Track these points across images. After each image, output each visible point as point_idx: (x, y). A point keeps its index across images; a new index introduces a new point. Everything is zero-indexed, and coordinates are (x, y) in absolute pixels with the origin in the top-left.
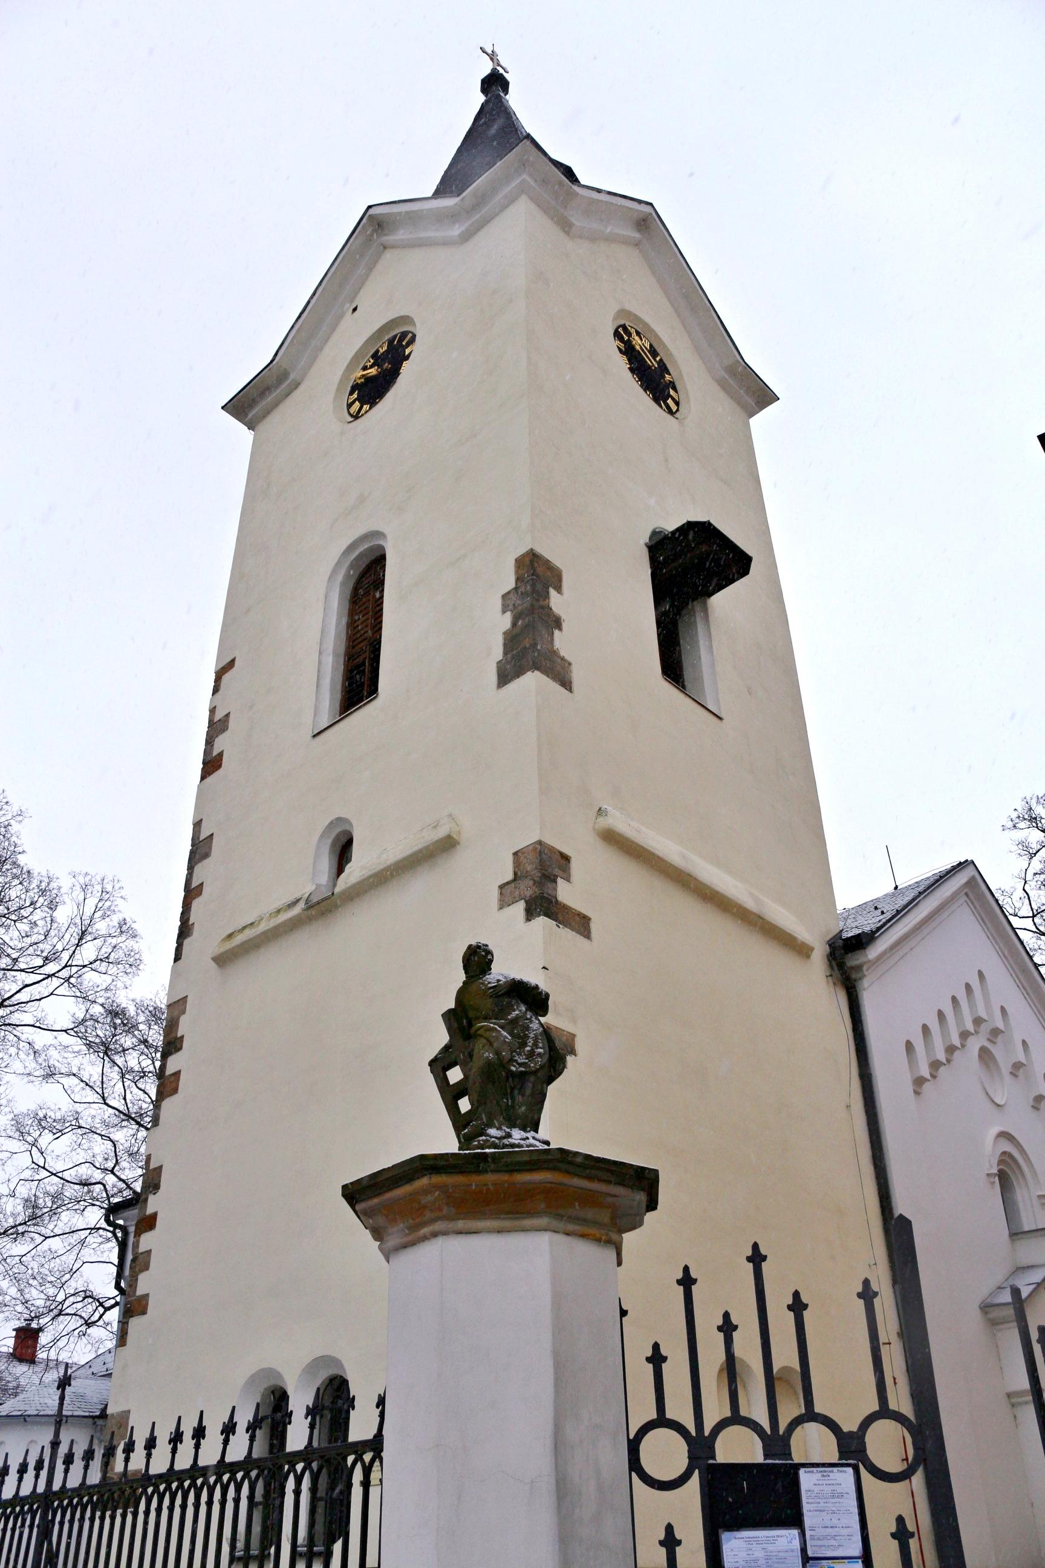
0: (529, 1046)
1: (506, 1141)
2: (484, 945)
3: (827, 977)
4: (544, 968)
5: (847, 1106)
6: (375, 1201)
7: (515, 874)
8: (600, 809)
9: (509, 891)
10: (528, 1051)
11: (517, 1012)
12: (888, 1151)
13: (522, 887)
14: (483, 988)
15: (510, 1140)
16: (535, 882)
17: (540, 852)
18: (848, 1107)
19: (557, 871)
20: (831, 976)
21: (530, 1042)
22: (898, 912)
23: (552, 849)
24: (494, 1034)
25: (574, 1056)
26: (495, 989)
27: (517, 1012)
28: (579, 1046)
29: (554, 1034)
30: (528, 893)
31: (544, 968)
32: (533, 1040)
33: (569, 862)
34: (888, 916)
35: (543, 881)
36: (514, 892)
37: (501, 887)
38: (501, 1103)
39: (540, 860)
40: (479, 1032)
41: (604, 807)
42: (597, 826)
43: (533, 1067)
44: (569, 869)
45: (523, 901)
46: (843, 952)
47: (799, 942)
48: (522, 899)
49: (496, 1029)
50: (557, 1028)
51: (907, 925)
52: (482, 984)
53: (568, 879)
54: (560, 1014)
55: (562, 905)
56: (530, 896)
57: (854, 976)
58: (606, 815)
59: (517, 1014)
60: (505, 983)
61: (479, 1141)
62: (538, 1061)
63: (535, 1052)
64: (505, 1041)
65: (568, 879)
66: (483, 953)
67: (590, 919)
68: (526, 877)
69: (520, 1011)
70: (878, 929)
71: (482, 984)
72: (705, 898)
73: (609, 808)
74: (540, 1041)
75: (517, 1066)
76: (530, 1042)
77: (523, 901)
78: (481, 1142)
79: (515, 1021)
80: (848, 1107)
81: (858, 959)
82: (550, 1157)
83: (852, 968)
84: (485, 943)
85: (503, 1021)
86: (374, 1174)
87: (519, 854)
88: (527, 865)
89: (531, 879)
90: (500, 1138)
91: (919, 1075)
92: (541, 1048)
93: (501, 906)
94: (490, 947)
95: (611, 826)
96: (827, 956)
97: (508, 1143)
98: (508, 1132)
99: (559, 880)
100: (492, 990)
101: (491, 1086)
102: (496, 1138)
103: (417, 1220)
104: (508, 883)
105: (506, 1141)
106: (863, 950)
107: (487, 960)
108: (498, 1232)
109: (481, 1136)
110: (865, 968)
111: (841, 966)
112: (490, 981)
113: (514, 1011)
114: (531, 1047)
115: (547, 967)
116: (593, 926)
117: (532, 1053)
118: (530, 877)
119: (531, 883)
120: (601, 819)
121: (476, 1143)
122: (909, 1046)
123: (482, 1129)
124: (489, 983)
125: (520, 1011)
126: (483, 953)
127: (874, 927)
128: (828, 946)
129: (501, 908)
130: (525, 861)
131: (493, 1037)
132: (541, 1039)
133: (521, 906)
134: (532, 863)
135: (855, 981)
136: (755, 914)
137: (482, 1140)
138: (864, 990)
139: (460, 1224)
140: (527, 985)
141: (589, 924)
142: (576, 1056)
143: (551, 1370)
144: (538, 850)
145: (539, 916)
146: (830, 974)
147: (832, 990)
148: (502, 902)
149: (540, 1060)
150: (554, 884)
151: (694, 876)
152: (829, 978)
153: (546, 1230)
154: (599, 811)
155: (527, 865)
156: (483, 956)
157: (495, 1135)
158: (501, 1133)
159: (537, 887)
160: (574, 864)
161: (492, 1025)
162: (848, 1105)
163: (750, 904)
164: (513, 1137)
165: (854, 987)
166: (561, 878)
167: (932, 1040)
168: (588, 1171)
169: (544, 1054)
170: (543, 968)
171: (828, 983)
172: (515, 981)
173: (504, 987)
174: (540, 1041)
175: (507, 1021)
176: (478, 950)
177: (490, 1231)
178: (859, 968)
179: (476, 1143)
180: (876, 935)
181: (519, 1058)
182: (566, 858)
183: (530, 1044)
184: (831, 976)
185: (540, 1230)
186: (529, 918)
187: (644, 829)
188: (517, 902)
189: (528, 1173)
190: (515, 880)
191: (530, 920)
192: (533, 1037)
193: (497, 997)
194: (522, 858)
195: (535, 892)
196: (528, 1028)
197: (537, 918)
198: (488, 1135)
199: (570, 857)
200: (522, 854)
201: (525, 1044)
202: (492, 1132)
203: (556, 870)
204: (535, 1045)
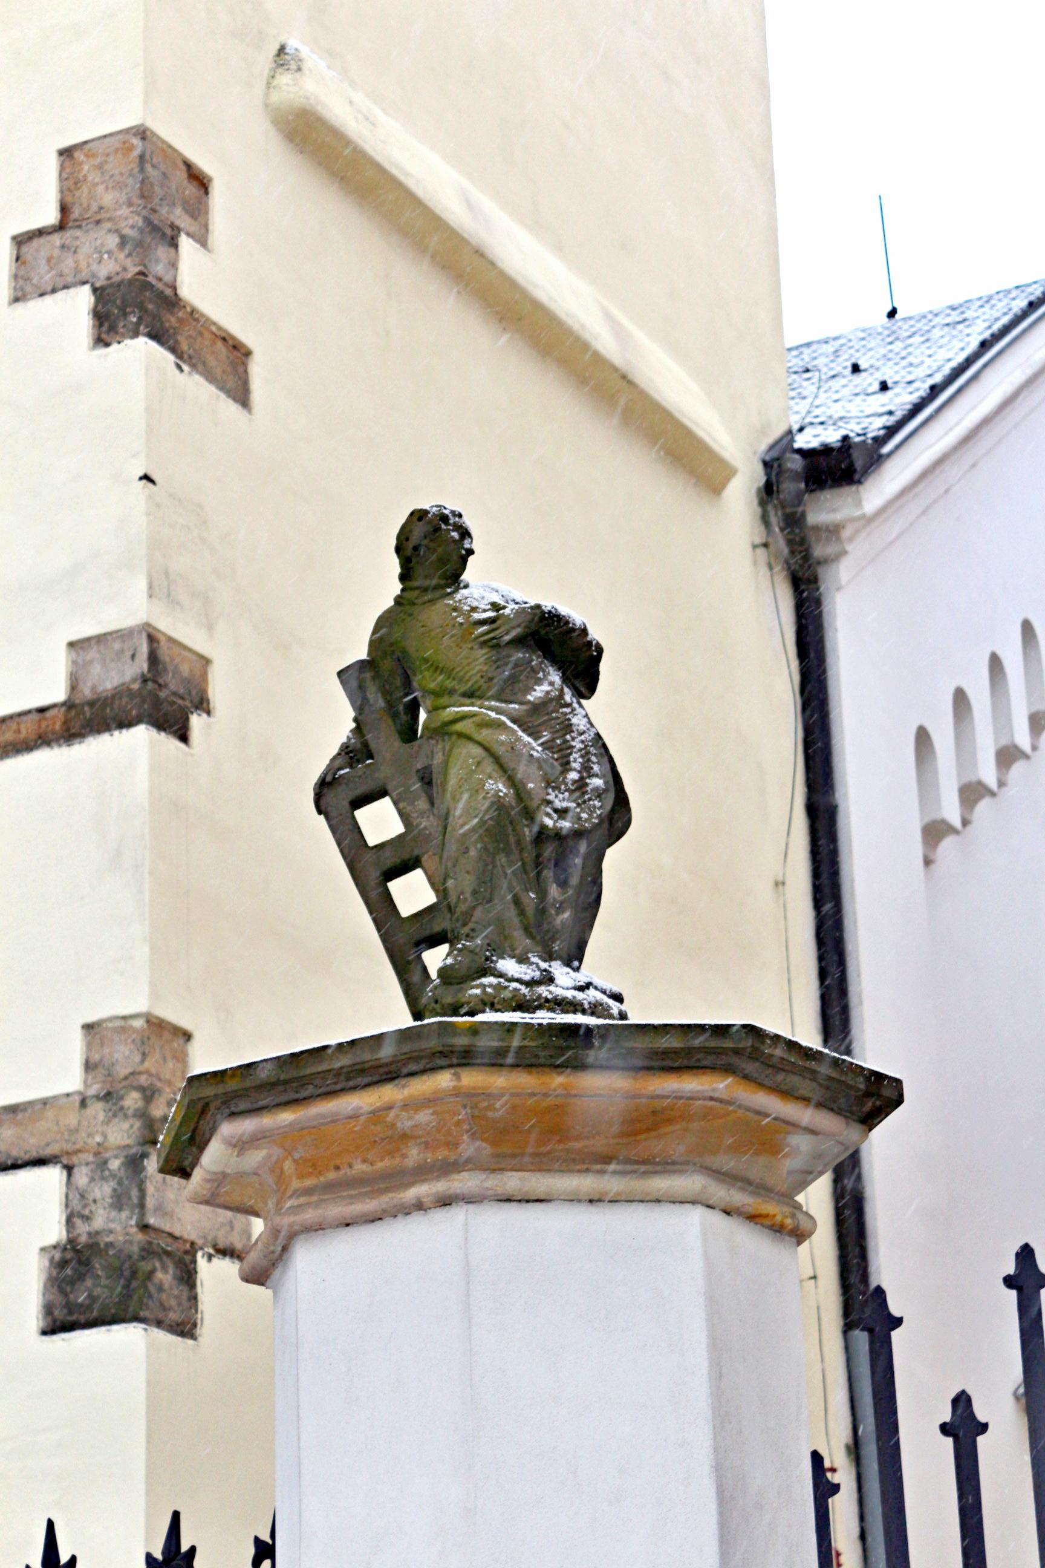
0: (575, 770)
1: (543, 991)
2: (453, 512)
3: (755, 547)
4: (146, 477)
5: (777, 884)
6: (286, 1117)
7: (64, 209)
8: (282, 50)
9: (44, 254)
10: (575, 782)
11: (545, 687)
12: (861, 1003)
13: (85, 250)
14: (460, 620)
15: (552, 988)
16: (124, 241)
17: (142, 157)
18: (779, 884)
19: (183, 220)
20: (765, 545)
21: (576, 764)
22: (935, 391)
23: (168, 151)
24: (503, 738)
25: (205, 715)
26: (493, 626)
27: (545, 687)
28: (218, 690)
29: (165, 652)
30: (106, 270)
31: (146, 477)
32: (582, 756)
33: (207, 193)
34: (901, 399)
35: (148, 239)
36: (60, 260)
37: (21, 241)
38: (525, 901)
39: (142, 182)
40: (459, 727)
41: (292, 44)
42: (275, 98)
43: (586, 820)
44: (207, 213)
45: (87, 288)
46: (803, 486)
47: (844, 483)
48: (84, 283)
49: (504, 723)
50: (171, 640)
51: (951, 429)
52: (455, 609)
53: (203, 241)
54: (178, 603)
55: (189, 309)
56: (109, 278)
57: (818, 551)
58: (299, 69)
59: (548, 693)
60: (519, 613)
61: (483, 986)
62: (594, 807)
63: (587, 785)
64: (532, 755)
65: (203, 241)
66: (455, 535)
67: (248, 353)
68: (98, 222)
69: (552, 684)
70: (891, 431)
71: (455, 609)
72: (502, 319)
73: (305, 51)
74: (594, 759)
75: (555, 816)
76: (576, 764)
77: (87, 288)
78: (489, 990)
79: (537, 708)
80: (779, 884)
81: (834, 511)
82: (728, 1044)
83: (817, 528)
84: (457, 509)
85: (517, 706)
86: (295, 1058)
87: (79, 155)
88: (101, 188)
89: (110, 231)
90: (531, 983)
91: (938, 817)
92: (597, 776)
93: (20, 294)
94: (468, 521)
95: (312, 101)
96: (759, 490)
97: (550, 997)
98: (545, 970)
99: (184, 242)
100: (485, 628)
101: (504, 860)
102: (518, 980)
103: (380, 1165)
104: (40, 233)
105: (543, 991)
106: (854, 488)
107: (463, 552)
108: (591, 1201)
109: (484, 975)
110: (846, 533)
111: (793, 522)
112: (475, 604)
113: (539, 682)
114: (579, 772)
115: (154, 477)
116: (257, 371)
117: (581, 785)
118: (107, 225)
119: (113, 241)
120: (284, 79)
121: (478, 991)
122: (923, 737)
123: (487, 959)
124: (474, 609)
125: (552, 684)
126: (455, 535)
127: (876, 426)
128: (760, 469)
129: (16, 300)
130: (94, 177)
131: (502, 743)
132: (595, 755)
133: (83, 299)
134: (119, 186)
135: (819, 563)
136: (616, 369)
137: (490, 986)
138: (839, 589)
139: (512, 1182)
140: (567, 622)
141: (245, 365)
142: (208, 713)
143: (712, 1507)
144: (136, 153)
145: (135, 334)
146: (764, 541)
147: (766, 583)
148: (21, 282)
149: (597, 804)
150: (172, 251)
151: (491, 257)
152: (761, 551)
153: (693, 1202)
154: (278, 55)
155: (101, 188)
156: (454, 541)
157: (517, 976)
158: (529, 971)
159: (129, 255)
160: (219, 198)
161: (493, 714)
162: (780, 878)
163: (606, 343)
164: (557, 981)
165: (814, 580)
166: (188, 234)
167: (973, 729)
168: (780, 1077)
169: (605, 791)
170: (141, 479)
171: (755, 563)
172: (543, 612)
173: (514, 623)
174: (594, 759)
175: (524, 707)
176: (443, 526)
177: (573, 1199)
178: (834, 531)
179: (478, 991)
180: (886, 449)
181: (556, 796)
182: (200, 181)
183: (576, 766)
184: (765, 545)
185: (674, 1202)
186: (104, 336)
187: (381, 116)
188: (66, 287)
189: (674, 1075)
190: (61, 227)
191: (107, 345)
192: (580, 750)
193: (493, 647)
194: (86, 167)
195: (125, 269)
196: (568, 727)
197: (128, 342)
198: (501, 975)
199: (210, 180)
200: (87, 156)
201: (566, 766)
202: (508, 966)
203: (178, 211)
204: (586, 768)
